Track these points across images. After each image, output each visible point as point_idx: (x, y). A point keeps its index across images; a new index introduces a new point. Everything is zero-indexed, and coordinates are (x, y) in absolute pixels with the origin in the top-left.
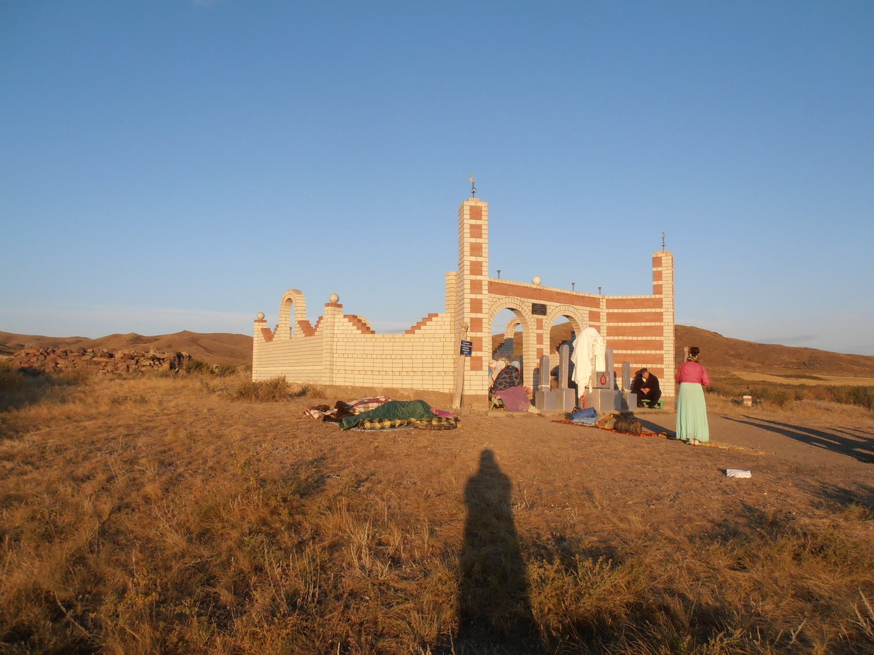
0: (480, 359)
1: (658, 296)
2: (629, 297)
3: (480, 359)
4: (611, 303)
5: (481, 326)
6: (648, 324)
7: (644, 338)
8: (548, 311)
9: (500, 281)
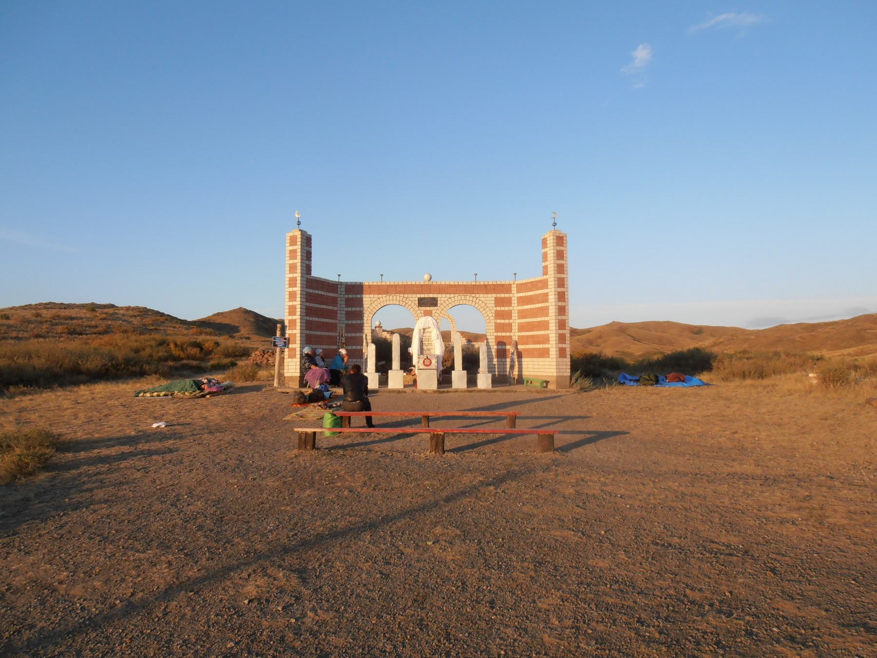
0: (294, 349)
1: (545, 277)
3: (294, 349)
4: (522, 287)
9: (383, 283)
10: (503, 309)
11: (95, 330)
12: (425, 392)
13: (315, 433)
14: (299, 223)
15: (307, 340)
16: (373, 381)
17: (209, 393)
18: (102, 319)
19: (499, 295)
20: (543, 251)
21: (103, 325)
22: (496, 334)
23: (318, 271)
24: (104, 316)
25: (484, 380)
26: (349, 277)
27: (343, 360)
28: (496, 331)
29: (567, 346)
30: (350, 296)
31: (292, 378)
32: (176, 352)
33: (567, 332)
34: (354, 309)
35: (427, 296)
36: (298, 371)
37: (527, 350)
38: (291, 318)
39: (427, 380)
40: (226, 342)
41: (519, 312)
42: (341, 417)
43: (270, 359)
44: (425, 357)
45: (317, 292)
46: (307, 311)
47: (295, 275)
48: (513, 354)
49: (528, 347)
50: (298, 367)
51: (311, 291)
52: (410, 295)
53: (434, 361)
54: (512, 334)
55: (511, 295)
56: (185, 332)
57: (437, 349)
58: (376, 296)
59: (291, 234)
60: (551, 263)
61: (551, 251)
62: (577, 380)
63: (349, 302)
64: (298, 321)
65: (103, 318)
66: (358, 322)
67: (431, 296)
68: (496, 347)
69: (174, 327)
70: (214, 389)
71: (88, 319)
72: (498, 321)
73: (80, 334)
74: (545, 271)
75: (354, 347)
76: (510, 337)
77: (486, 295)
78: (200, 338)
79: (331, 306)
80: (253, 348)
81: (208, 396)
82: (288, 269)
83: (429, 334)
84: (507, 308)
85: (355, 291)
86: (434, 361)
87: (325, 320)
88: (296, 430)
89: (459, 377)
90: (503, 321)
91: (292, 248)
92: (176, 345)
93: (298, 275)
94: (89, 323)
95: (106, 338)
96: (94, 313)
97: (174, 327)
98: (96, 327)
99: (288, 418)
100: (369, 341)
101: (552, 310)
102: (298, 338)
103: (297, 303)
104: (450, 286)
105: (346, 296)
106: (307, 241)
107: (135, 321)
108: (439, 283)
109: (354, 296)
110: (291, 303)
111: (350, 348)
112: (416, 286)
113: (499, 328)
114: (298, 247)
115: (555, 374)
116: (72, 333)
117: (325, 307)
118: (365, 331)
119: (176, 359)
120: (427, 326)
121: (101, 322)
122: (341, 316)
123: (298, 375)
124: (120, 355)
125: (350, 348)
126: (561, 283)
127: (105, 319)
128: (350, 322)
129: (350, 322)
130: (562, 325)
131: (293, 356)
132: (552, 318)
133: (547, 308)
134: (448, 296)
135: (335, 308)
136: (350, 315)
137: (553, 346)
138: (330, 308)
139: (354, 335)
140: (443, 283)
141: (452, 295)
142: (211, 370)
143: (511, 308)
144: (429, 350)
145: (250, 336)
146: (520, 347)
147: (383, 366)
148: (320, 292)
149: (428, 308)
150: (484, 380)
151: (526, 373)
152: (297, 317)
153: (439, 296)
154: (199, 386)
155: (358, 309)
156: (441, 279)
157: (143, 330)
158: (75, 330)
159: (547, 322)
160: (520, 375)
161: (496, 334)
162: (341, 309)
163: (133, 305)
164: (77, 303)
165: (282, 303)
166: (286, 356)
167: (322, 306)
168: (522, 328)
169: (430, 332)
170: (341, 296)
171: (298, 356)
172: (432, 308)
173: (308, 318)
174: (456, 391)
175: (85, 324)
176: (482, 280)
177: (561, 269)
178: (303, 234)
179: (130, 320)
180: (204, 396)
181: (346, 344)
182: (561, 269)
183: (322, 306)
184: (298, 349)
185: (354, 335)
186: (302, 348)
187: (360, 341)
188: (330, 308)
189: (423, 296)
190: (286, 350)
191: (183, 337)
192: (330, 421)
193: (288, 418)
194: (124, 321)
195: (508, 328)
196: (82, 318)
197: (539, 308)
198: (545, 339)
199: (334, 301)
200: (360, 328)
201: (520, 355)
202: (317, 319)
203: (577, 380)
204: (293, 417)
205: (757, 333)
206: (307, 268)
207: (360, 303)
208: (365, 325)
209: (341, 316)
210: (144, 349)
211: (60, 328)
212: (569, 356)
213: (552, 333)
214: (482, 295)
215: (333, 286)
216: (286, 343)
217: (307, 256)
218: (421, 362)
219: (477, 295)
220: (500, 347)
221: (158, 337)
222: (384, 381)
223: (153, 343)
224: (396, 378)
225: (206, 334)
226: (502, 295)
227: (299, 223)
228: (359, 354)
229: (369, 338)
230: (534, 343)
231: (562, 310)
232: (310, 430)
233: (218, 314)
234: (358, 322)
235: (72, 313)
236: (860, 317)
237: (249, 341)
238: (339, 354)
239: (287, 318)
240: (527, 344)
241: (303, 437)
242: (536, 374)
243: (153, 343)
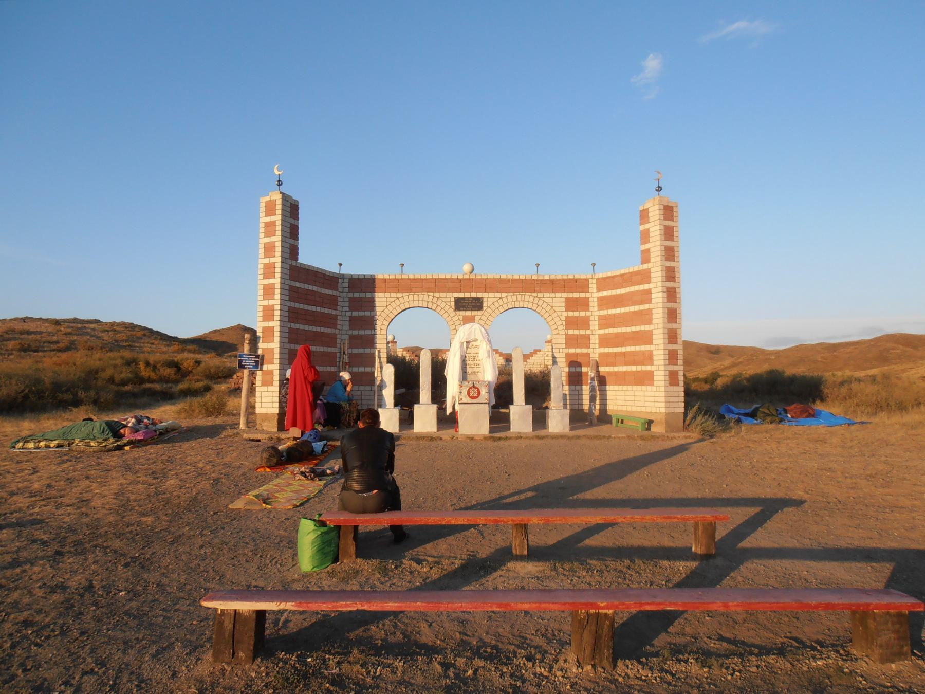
0: (271, 372)
1: (645, 266)
2: (618, 273)
3: (271, 372)
4: (603, 283)
5: (599, 339)
6: (637, 308)
7: (633, 329)
8: (485, 304)
9: (405, 277)
10: (576, 314)
11: (53, 347)
12: (472, 438)
13: (261, 615)
14: (280, 183)
15: (288, 358)
16: (389, 419)
17: (130, 443)
18: (66, 334)
19: (571, 295)
20: (642, 228)
22: (567, 351)
23: (305, 258)
24: (69, 330)
25: (558, 420)
26: (353, 268)
27: (345, 388)
28: (568, 345)
29: (679, 368)
30: (357, 295)
31: (266, 417)
32: (145, 373)
33: (679, 348)
34: (361, 314)
35: (467, 295)
36: (277, 405)
37: (616, 374)
38: (265, 324)
39: (474, 422)
40: (211, 360)
41: (601, 318)
42: (338, 528)
44: (471, 384)
45: (306, 286)
46: (291, 315)
47: (273, 260)
48: (592, 379)
49: (616, 369)
50: (277, 400)
51: (298, 285)
52: (443, 294)
53: (484, 391)
54: (590, 351)
55: (588, 295)
56: (165, 349)
57: (488, 374)
58: (394, 295)
59: (267, 199)
60: (656, 246)
61: (655, 228)
62: (694, 418)
63: (355, 304)
64: (277, 329)
65: (76, 333)
66: (368, 332)
67: (474, 295)
68: (567, 369)
69: (152, 344)
70: (139, 436)
71: (49, 334)
72: (571, 332)
73: (36, 351)
74: (646, 257)
75: (361, 369)
76: (588, 355)
77: (552, 295)
78: (178, 357)
79: (327, 311)
81: (127, 448)
82: (262, 251)
83: (474, 351)
84: (582, 314)
85: (363, 288)
86: (484, 391)
87: (318, 329)
88: (205, 604)
89: (520, 412)
90: (576, 332)
91: (268, 219)
92: (147, 364)
93: (277, 260)
94: (49, 338)
95: (64, 356)
96: (58, 328)
97: (152, 344)
98: (57, 342)
99: (239, 504)
100: (384, 360)
101: (659, 315)
102: (277, 356)
103: (276, 302)
104: (501, 281)
105: (350, 295)
106: (291, 210)
107: (105, 336)
108: (485, 277)
109: (362, 295)
110: (266, 303)
111: (355, 369)
112: (452, 280)
113: (571, 341)
114: (278, 218)
115: (663, 410)
116: (25, 349)
117: (318, 309)
118: (378, 346)
119: (142, 381)
120: (472, 337)
121: (64, 337)
122: (343, 323)
123: (277, 411)
124: (47, 378)
125: (355, 369)
126: (670, 275)
127: (70, 334)
128: (356, 332)
129: (356, 332)
130: (672, 336)
131: (267, 383)
132: (658, 327)
133: (649, 312)
134: (498, 295)
135: (334, 312)
136: (355, 323)
137: (659, 369)
138: (326, 311)
139: (361, 351)
140: (491, 277)
141: (504, 295)
142: (179, 396)
143: (588, 313)
144: (475, 373)
146: (602, 369)
147: (406, 398)
148: (311, 288)
149: (469, 313)
150: (558, 420)
151: (611, 407)
152: (276, 324)
153: (485, 295)
154: (115, 430)
155: (367, 313)
156: (487, 272)
157: (115, 346)
159: (650, 333)
160: (603, 410)
161: (567, 351)
162: (343, 313)
163: (118, 320)
164: (35, 317)
165: (251, 302)
166: (258, 382)
167: (314, 308)
168: (605, 341)
169: (476, 347)
170: (343, 294)
171: (276, 383)
172: (474, 313)
173: (293, 326)
174: (519, 437)
175: (44, 339)
176: (547, 273)
177: (670, 253)
178: (285, 198)
179: (100, 334)
180: (120, 448)
181: (350, 364)
182: (670, 253)
183: (314, 308)
184: (277, 372)
185: (361, 351)
186: (282, 370)
187: (370, 360)
188: (326, 311)
189: (461, 295)
190: (259, 373)
191: (159, 354)
192: (312, 536)
193: (239, 504)
194: (92, 336)
195: (584, 341)
196: (41, 333)
197: (635, 313)
198: (648, 358)
199: (333, 302)
200: (370, 341)
201: (602, 381)
202: (306, 327)
203: (694, 418)
204: (250, 502)
205: (777, 353)
206: (291, 251)
207: (370, 304)
208: (378, 336)
209: (343, 323)
210: (103, 370)
211: (11, 345)
212: (682, 383)
213: (659, 348)
214: (546, 295)
215: (330, 280)
216: (259, 362)
217: (291, 232)
218: (465, 392)
219: (540, 295)
220: (573, 369)
221: (127, 354)
222: (407, 420)
223: (119, 362)
224: (425, 417)
225: (190, 351)
226: (576, 295)
227: (280, 183)
228: (366, 380)
229: (384, 356)
230: (626, 364)
231: (672, 315)
232: (246, 607)
233: (215, 331)
235: (32, 327)
236: (882, 337)
238: (340, 379)
239: (259, 326)
240: (614, 365)
241: (228, 624)
242: (629, 409)
243: (119, 362)
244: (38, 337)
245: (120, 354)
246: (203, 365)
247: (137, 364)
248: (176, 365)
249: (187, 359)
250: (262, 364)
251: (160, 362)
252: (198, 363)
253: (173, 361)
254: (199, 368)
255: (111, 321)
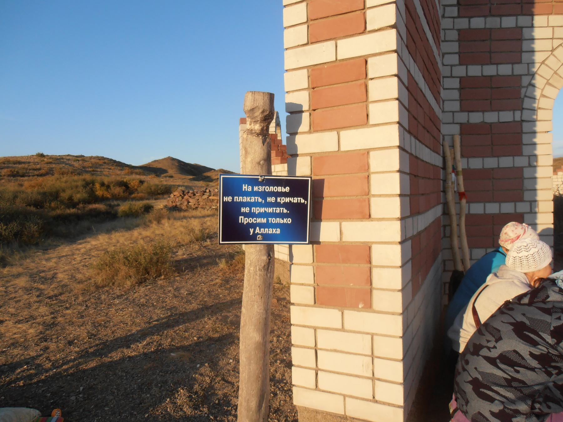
0: (364, 253)
3: (364, 253)
18: (47, 163)
21: (46, 167)
30: (478, 23)
34: (490, 70)
40: (152, 181)
43: (191, 200)
69: (110, 169)
73: (23, 176)
78: (126, 179)
80: (174, 185)
92: (103, 184)
94: (34, 167)
95: (40, 179)
97: (110, 169)
98: (40, 169)
105: (463, 23)
107: (76, 164)
116: (15, 175)
121: (45, 165)
127: (51, 163)
128: (476, 118)
129: (476, 118)
131: (346, 290)
139: (491, 163)
145: (173, 175)
158: (18, 172)
163: (94, 155)
166: (300, 294)
175: (30, 167)
185: (491, 163)
194: (66, 164)
196: (29, 163)
210: (64, 191)
211: (4, 172)
221: (88, 177)
223: (80, 183)
225: (136, 173)
233: (155, 161)
234: (506, 116)
237: (172, 179)
244: (26, 166)
245: (83, 177)
246: (145, 184)
247: (93, 185)
248: (125, 185)
249: (133, 180)
250: (317, 217)
251: (112, 182)
252: (142, 182)
253: (123, 181)
254: (142, 187)
255: (90, 156)
